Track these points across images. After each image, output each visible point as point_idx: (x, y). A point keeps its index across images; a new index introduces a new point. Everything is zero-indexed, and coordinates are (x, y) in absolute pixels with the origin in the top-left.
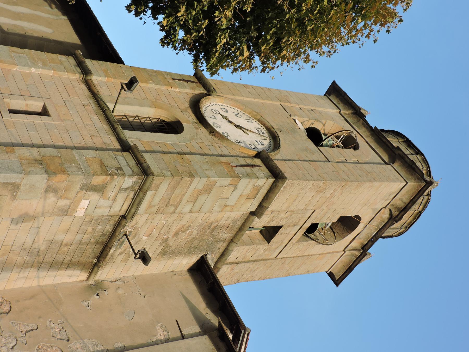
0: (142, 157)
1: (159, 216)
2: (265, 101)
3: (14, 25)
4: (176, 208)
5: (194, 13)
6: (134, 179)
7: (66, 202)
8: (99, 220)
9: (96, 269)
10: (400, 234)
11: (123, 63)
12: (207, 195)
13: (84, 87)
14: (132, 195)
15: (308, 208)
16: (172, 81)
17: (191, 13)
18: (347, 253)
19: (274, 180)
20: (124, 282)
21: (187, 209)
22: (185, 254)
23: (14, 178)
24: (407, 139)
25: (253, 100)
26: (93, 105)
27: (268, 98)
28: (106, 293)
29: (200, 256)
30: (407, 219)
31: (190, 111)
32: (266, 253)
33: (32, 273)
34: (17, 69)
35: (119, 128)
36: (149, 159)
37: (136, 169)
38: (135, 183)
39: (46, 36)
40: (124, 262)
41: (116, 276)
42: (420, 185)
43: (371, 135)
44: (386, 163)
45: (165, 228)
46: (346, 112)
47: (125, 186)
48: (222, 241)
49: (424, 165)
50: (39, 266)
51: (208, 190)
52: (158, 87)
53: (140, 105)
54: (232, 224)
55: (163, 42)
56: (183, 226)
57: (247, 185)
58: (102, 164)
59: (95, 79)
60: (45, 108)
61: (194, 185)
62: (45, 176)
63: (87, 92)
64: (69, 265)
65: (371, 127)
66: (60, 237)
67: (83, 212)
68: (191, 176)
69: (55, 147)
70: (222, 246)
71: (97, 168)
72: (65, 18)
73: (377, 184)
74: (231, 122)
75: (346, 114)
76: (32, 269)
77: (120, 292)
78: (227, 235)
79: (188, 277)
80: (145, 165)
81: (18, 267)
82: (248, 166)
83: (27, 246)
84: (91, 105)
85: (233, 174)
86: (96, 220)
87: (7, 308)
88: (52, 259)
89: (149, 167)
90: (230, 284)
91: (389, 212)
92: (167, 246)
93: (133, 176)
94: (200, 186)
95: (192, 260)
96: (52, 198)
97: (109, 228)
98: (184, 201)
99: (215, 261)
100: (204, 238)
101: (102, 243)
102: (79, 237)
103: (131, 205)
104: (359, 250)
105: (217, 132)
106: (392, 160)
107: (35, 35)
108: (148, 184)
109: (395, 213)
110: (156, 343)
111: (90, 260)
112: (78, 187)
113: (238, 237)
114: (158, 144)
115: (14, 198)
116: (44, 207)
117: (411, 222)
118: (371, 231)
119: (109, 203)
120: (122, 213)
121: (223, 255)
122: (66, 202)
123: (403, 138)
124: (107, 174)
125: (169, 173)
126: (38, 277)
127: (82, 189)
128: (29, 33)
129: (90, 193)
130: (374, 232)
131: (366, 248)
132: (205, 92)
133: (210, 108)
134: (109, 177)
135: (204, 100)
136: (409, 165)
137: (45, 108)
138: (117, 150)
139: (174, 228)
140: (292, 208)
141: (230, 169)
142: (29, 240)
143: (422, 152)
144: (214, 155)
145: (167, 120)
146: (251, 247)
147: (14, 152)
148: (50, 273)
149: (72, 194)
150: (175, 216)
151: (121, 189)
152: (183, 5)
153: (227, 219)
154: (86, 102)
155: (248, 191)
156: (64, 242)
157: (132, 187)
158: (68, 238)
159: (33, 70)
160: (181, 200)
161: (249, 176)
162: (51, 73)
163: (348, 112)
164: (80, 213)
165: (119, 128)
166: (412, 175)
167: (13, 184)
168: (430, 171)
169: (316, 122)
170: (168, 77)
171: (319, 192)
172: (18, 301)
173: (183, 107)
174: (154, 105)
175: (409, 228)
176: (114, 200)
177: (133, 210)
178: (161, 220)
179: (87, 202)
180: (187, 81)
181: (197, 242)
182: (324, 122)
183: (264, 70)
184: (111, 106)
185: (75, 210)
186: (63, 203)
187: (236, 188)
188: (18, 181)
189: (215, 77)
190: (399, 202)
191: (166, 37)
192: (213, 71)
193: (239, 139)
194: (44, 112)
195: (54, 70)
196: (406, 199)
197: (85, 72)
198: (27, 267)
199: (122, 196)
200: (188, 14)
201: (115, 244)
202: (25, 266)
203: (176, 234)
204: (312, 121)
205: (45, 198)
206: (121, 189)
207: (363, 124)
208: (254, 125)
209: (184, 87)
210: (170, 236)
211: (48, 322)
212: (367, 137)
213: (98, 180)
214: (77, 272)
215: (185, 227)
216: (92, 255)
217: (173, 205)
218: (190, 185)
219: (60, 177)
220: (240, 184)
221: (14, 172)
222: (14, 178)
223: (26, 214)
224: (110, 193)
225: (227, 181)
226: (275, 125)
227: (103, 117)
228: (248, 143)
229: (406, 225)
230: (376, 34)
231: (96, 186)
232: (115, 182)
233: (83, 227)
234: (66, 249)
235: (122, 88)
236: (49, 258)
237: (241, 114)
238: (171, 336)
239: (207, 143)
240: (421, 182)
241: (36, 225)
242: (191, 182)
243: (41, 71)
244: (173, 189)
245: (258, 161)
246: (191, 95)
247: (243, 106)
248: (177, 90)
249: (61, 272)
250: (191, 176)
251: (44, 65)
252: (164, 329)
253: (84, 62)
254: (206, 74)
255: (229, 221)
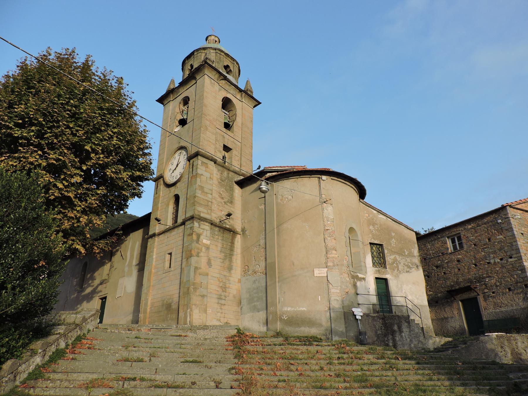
0: (187, 218)
1: (213, 208)
2: (166, 146)
3: (136, 258)
4: (210, 201)
5: (126, 187)
6: (195, 222)
7: (203, 248)
8: (213, 234)
9: (235, 232)
10: (237, 63)
11: (151, 213)
12: (205, 188)
13: (161, 236)
14: (202, 222)
15: (215, 133)
16: (158, 194)
17: (125, 188)
18: (243, 100)
19: (199, 156)
20: (243, 219)
21: (210, 196)
22: (233, 192)
23: (192, 269)
24: (186, 58)
25: (165, 153)
26: (168, 234)
27: (165, 143)
28: (246, 227)
29: (235, 184)
30: (229, 61)
31: (170, 188)
32: (237, 149)
33: (234, 258)
34: (154, 263)
35: (176, 224)
36: (188, 215)
37: (191, 221)
38: (197, 222)
39: (140, 245)
40: (233, 220)
41: (240, 222)
42: (207, 67)
43: (183, 86)
44: (196, 82)
45: (219, 204)
46: (171, 97)
47: (198, 226)
48: (228, 175)
49: (199, 52)
50: (231, 255)
51: (202, 188)
52: (160, 202)
53: (168, 213)
54: (220, 172)
55: (140, 197)
56: (219, 196)
57: (201, 169)
58: (189, 235)
59: (157, 231)
60: (169, 254)
61: (199, 195)
62: (192, 257)
63: (162, 235)
64: (232, 243)
65: (179, 86)
66: (219, 248)
67: (208, 241)
68: (195, 197)
69: (183, 252)
70: (231, 174)
71: (190, 237)
72: (131, 234)
73: (205, 94)
74: (175, 169)
75: (173, 97)
76: (233, 258)
77: (246, 221)
78: (226, 173)
79: (244, 189)
80: (190, 217)
81: (231, 263)
82: (193, 167)
83: (221, 261)
84: (167, 234)
85: (195, 176)
86: (213, 235)
87: (247, 267)
88: (229, 250)
89: (190, 216)
90: (252, 165)
91: (222, 81)
92: (228, 201)
93: (194, 223)
94: (200, 192)
95: (237, 188)
96: (202, 254)
97: (217, 229)
98: (206, 198)
99: (238, 176)
100: (226, 184)
101: (224, 231)
102: (220, 241)
103: (207, 222)
104: (242, 93)
105: (179, 179)
106: (195, 78)
107: (140, 249)
108: (197, 217)
109: (222, 77)
110: (265, 209)
111: (231, 235)
112: (197, 245)
113: (227, 167)
114: (183, 208)
115: (200, 268)
116: (204, 256)
117: (231, 58)
118: (232, 89)
119: (205, 231)
120: (210, 225)
121: (235, 173)
122: (203, 248)
123: (186, 60)
124: (192, 234)
125: (194, 207)
126: (237, 254)
127: (198, 243)
128: (139, 252)
129: (200, 239)
130: (233, 87)
131: (241, 90)
132: (162, 178)
133: (169, 178)
134: (194, 233)
135: (166, 181)
136: (197, 70)
137: (169, 254)
138: (185, 226)
139: (219, 199)
140: (214, 142)
141: (193, 177)
142: (219, 260)
143: (193, 51)
144: (188, 183)
145: (174, 200)
146: (233, 158)
147: (183, 268)
148: (235, 251)
149: (200, 246)
150: (214, 201)
151: (199, 227)
152: (122, 192)
153: (217, 174)
154: (166, 237)
155: (203, 168)
156: (222, 246)
157: (198, 223)
158: (220, 245)
159: (154, 257)
160: (206, 200)
161: (197, 169)
162: (155, 249)
163: (172, 96)
164: (208, 242)
165: (176, 224)
166: (202, 70)
167: (195, 269)
168: (203, 48)
169: (177, 118)
170: (156, 195)
171: (207, 129)
172: (245, 263)
173: (169, 192)
174: (168, 205)
175: (234, 59)
176: (204, 229)
177: (209, 221)
178: (214, 207)
179: (204, 240)
180: (157, 187)
181: (228, 188)
182: (176, 113)
183: (151, 148)
184: (168, 227)
185: (207, 245)
186: (204, 249)
187: (202, 175)
188: (194, 267)
189: (155, 173)
190: (216, 76)
191: (138, 196)
192: (152, 173)
193: (182, 167)
194: (170, 254)
195: (154, 248)
196: (214, 73)
197: (154, 235)
198: (232, 260)
199: (203, 226)
200: (126, 190)
201: (224, 225)
202: (231, 261)
203: (222, 198)
204: (176, 120)
205: (201, 256)
206: (199, 227)
207: (177, 89)
208: (177, 155)
209: (160, 189)
210: (223, 201)
211: (253, 252)
212: (184, 89)
213: (194, 237)
214: (236, 239)
215: (219, 194)
216: (229, 234)
217: (208, 203)
218: (199, 197)
219: (193, 252)
220: (200, 173)
221: (190, 269)
222: (192, 269)
223: (207, 263)
224: (200, 231)
225: (198, 180)
226: (177, 146)
227: (172, 230)
228: (184, 163)
229: (232, 61)
230: (130, 92)
231: (197, 238)
232: (196, 230)
233: (215, 240)
234: (225, 246)
235: (160, 223)
236: (228, 252)
237: (172, 162)
238: (264, 202)
239: (183, 184)
240: (205, 66)
241: (213, 258)
242: (198, 197)
243: (154, 254)
244: (201, 205)
245: (191, 161)
246: (164, 186)
247: (169, 159)
248: (161, 192)
249: (235, 246)
250: (195, 197)
251: (152, 252)
252: (261, 205)
253: (150, 235)
254: (155, 176)
255: (218, 173)
